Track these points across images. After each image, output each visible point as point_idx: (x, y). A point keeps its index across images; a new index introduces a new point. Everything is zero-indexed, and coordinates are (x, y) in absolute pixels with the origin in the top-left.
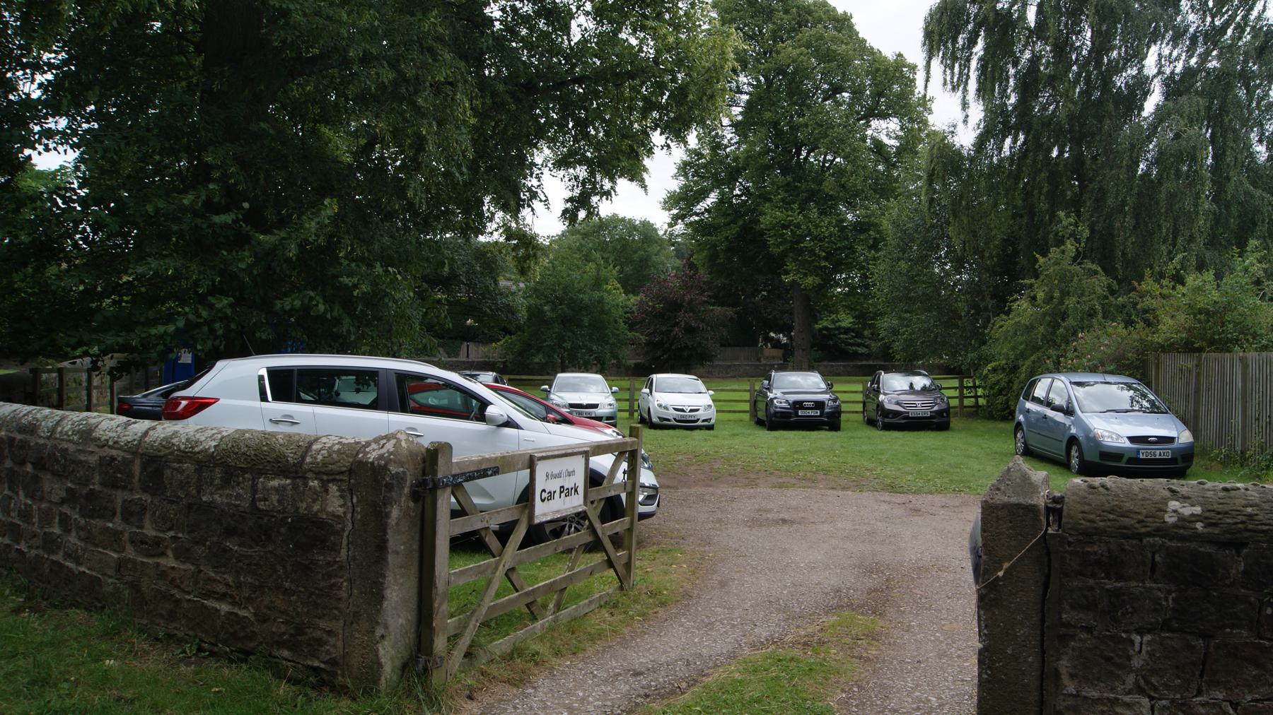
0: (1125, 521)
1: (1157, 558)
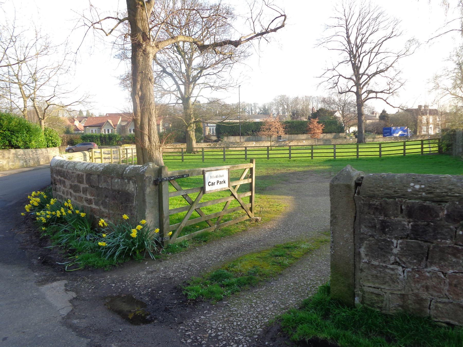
0: (387, 191)
1: (403, 207)
